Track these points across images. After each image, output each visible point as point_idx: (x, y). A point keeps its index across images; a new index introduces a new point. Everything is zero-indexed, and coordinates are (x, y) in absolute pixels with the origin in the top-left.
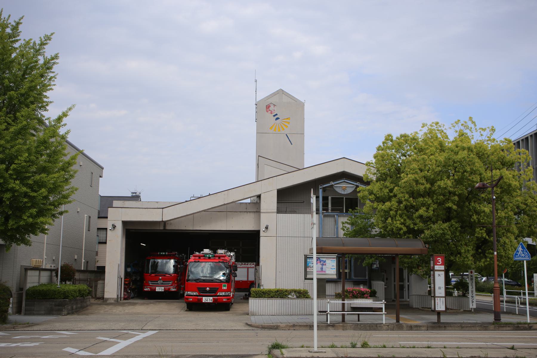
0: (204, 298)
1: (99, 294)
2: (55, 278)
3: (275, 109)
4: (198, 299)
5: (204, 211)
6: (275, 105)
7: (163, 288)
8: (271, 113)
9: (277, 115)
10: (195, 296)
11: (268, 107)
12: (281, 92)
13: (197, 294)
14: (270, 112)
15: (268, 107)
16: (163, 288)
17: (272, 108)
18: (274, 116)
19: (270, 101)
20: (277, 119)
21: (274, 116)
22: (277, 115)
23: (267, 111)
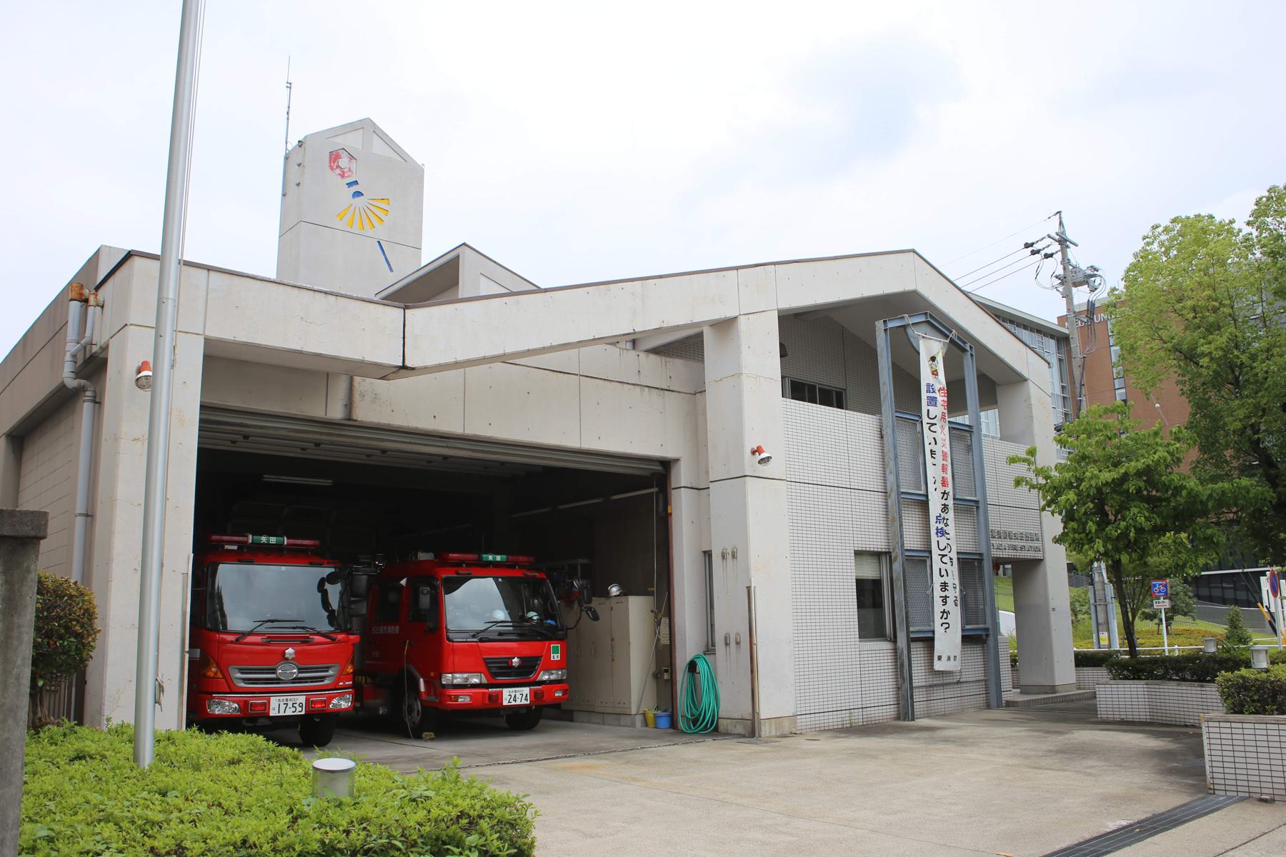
0: (506, 692)
1: (731, 705)
2: (326, 682)
3: (353, 168)
4: (490, 696)
5: (504, 358)
6: (352, 157)
7: (302, 699)
8: (343, 176)
9: (356, 183)
10: (474, 686)
11: (334, 157)
12: (366, 127)
13: (484, 681)
14: (338, 171)
15: (334, 157)
16: (302, 699)
17: (344, 162)
18: (350, 185)
19: (341, 142)
20: (358, 194)
21: (350, 185)
22: (356, 183)
23: (332, 169)
